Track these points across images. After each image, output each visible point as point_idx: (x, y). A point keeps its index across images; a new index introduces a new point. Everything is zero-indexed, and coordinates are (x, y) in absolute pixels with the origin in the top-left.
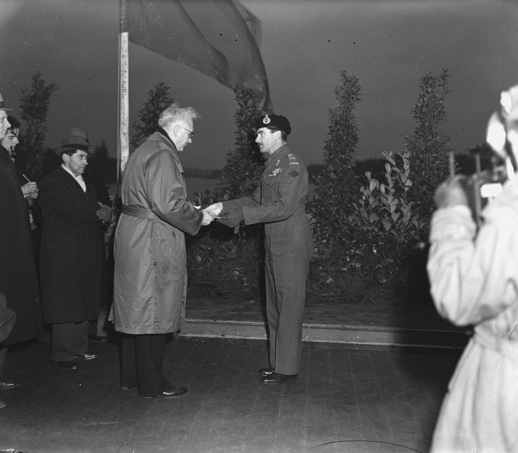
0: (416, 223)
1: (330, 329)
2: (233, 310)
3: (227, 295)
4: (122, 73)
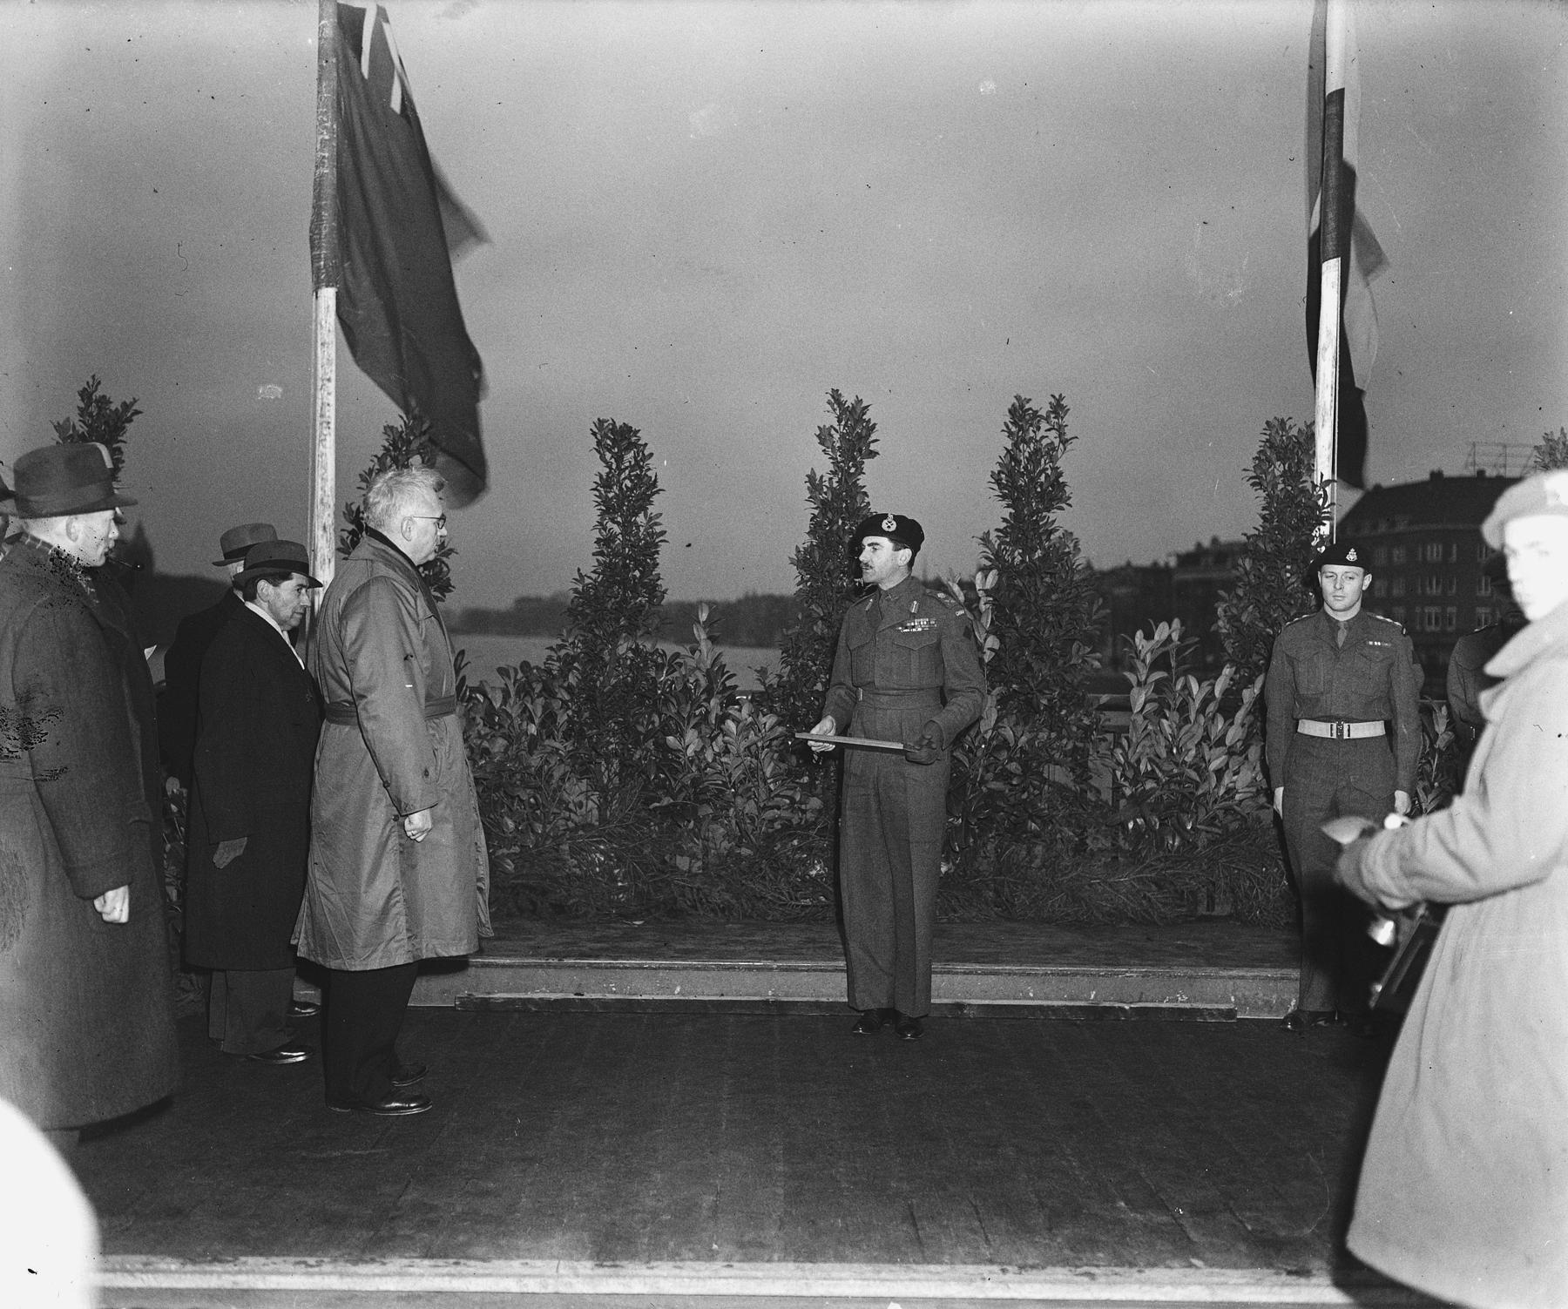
0: (1009, 734)
1: (821, 970)
2: (598, 940)
3: (577, 910)
4: (320, 383)
